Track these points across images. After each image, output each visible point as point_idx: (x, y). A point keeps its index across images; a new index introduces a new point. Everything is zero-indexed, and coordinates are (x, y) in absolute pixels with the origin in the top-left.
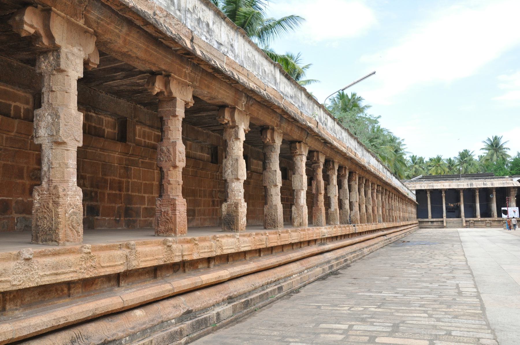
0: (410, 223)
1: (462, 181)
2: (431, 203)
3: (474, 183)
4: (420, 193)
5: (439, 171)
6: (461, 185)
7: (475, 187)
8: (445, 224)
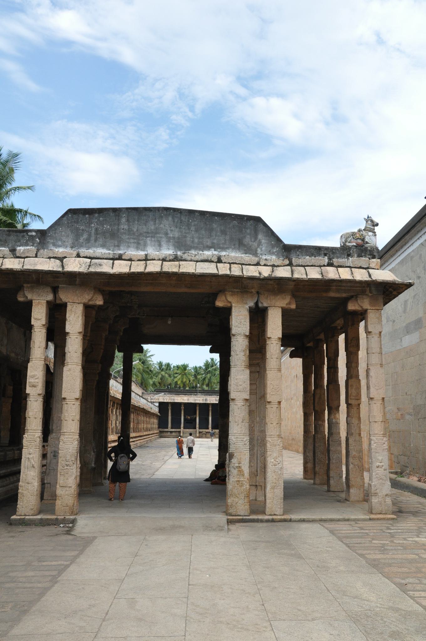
0: (151, 432)
1: (199, 396)
2: (172, 415)
3: (208, 399)
4: (163, 406)
5: (184, 380)
6: (198, 400)
7: (208, 402)
8: (182, 434)
